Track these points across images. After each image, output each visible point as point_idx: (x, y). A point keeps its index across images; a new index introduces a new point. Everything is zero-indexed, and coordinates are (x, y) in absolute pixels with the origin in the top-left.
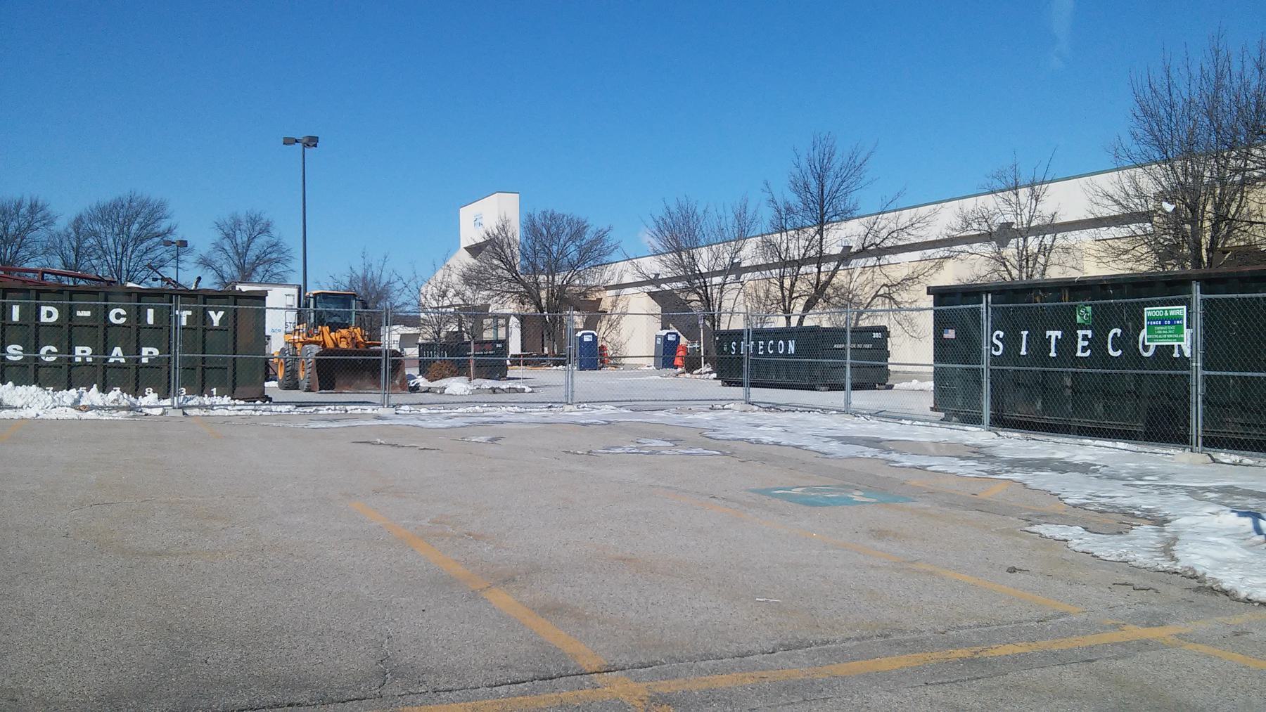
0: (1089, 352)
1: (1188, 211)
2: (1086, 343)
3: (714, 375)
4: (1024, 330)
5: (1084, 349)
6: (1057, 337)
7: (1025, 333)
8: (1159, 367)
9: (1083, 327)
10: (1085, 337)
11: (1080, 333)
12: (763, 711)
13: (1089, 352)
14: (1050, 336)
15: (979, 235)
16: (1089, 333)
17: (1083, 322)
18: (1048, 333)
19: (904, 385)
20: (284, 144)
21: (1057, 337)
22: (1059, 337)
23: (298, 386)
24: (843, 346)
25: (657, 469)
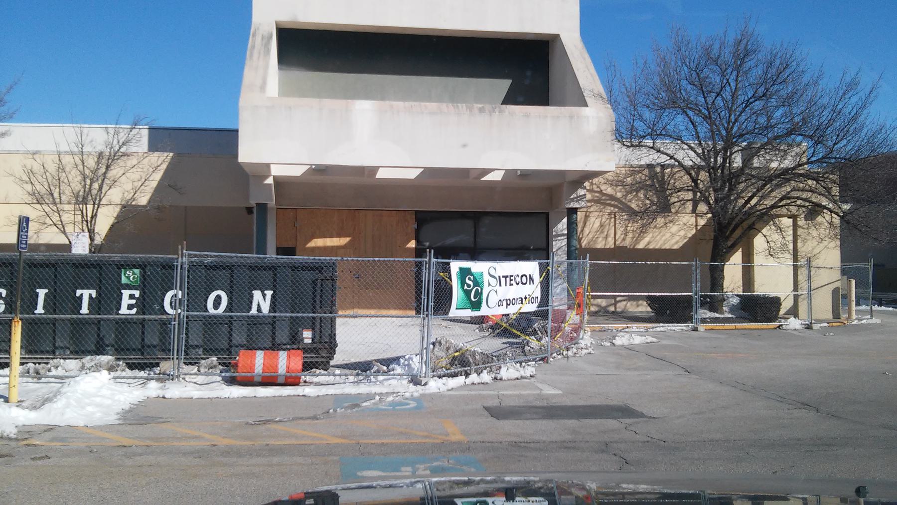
0: (134, 311)
1: (782, 177)
2: (133, 302)
3: (628, 247)
4: (41, 287)
5: (130, 307)
6: (90, 295)
7: (42, 293)
8: (67, 311)
9: (128, 287)
10: (132, 297)
11: (126, 293)
12: (106, 504)
13: (134, 311)
14: (82, 295)
15: (619, 418)
16: (137, 293)
17: (129, 283)
18: (79, 292)
19: (429, 492)
20: (457, 309)
21: (90, 295)
22: (94, 296)
23: (710, 267)
24: (176, 256)
25: (22, 74)
